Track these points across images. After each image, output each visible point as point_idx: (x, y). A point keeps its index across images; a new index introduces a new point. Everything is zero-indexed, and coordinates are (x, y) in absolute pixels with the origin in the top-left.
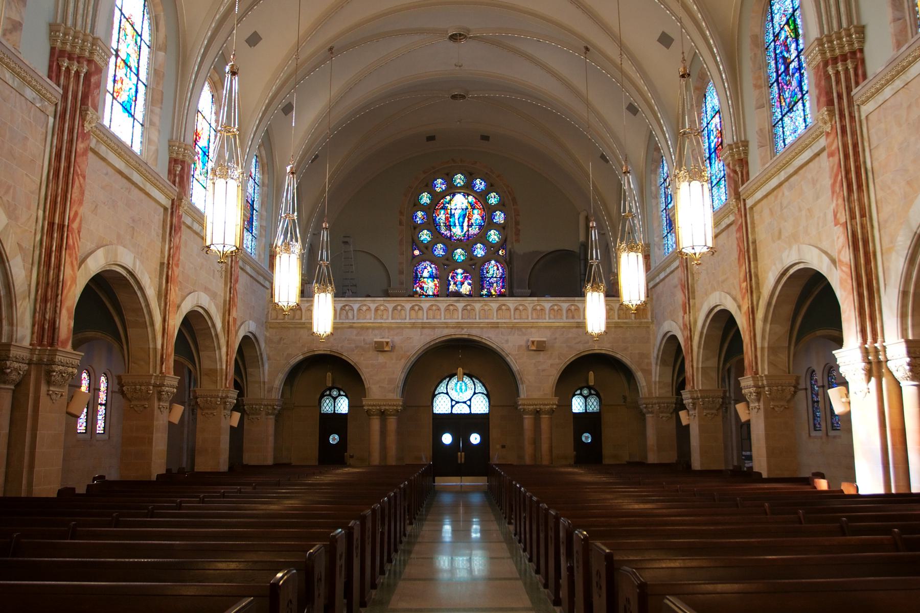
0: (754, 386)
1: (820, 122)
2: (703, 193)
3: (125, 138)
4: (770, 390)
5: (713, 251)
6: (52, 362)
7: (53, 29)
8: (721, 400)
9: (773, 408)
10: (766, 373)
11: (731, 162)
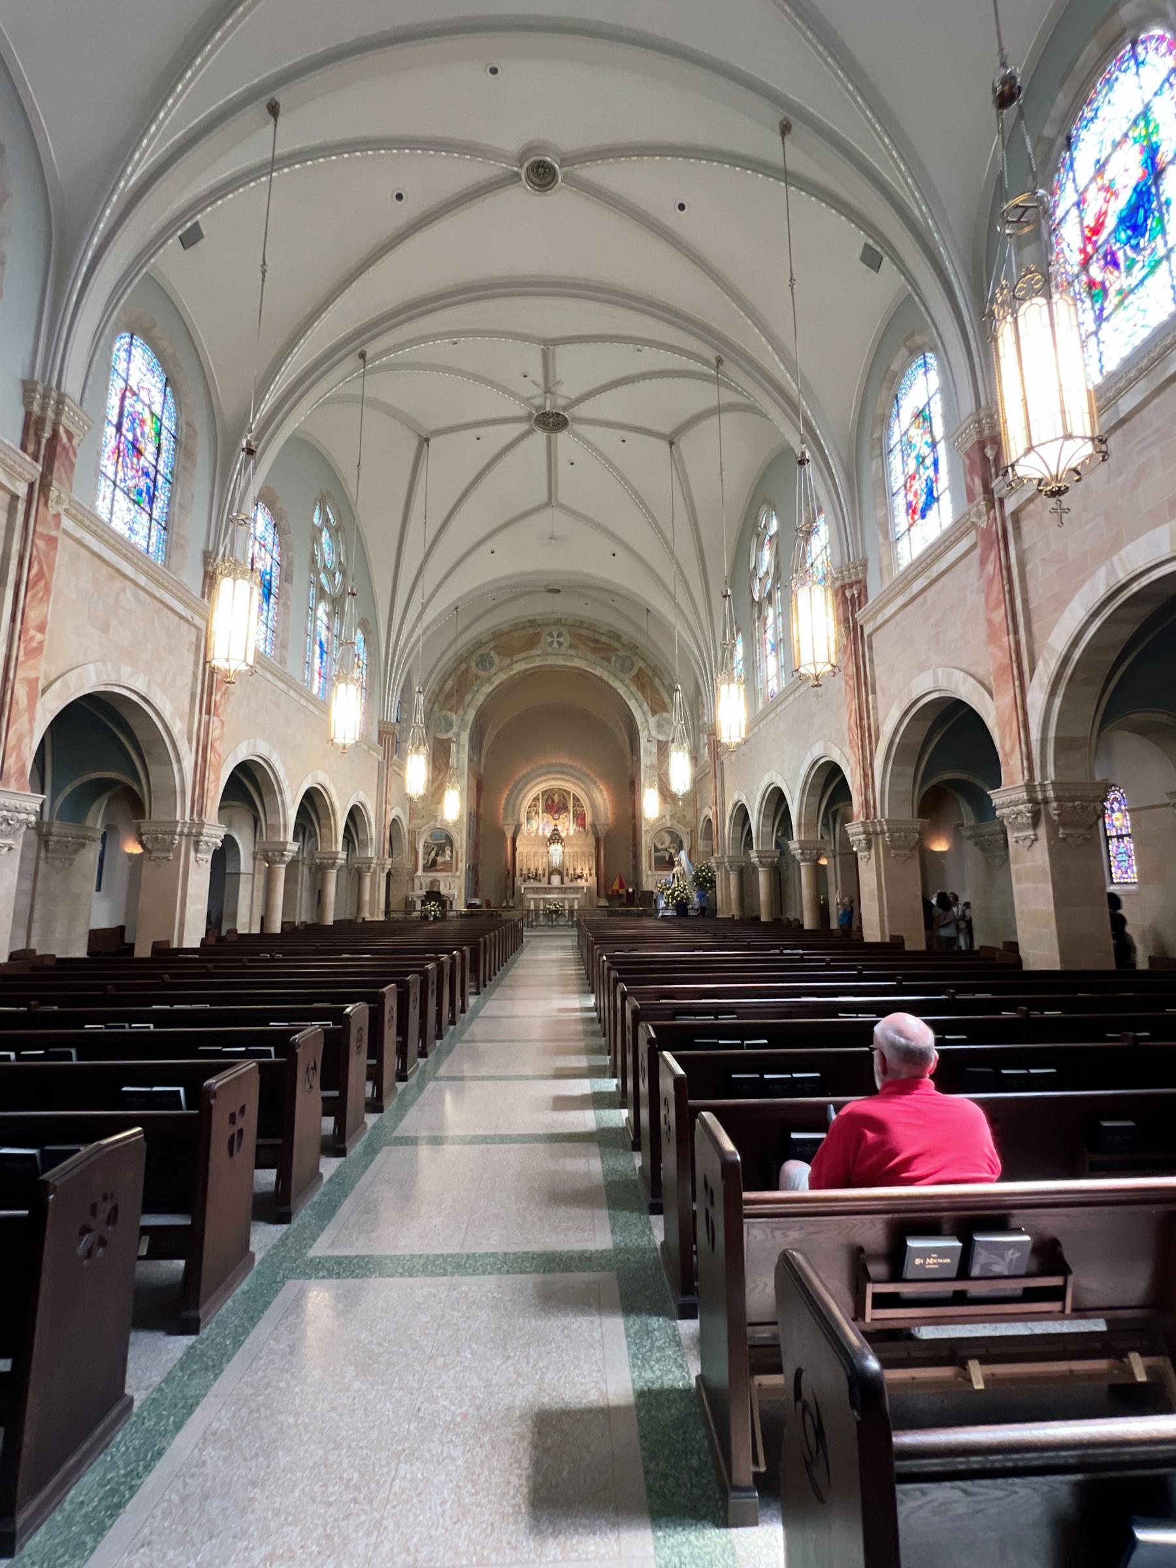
0: (1029, 801)
1: (972, 516)
2: (1055, 342)
3: (140, 541)
4: (1059, 808)
5: (746, 741)
6: (200, 834)
7: (380, 722)
8: (917, 836)
9: (1064, 839)
10: (887, 817)
11: (901, 519)
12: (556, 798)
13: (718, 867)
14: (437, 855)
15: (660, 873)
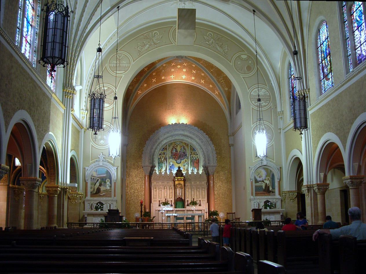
12: (179, 149)
13: (308, 190)
14: (100, 185)
15: (258, 197)
